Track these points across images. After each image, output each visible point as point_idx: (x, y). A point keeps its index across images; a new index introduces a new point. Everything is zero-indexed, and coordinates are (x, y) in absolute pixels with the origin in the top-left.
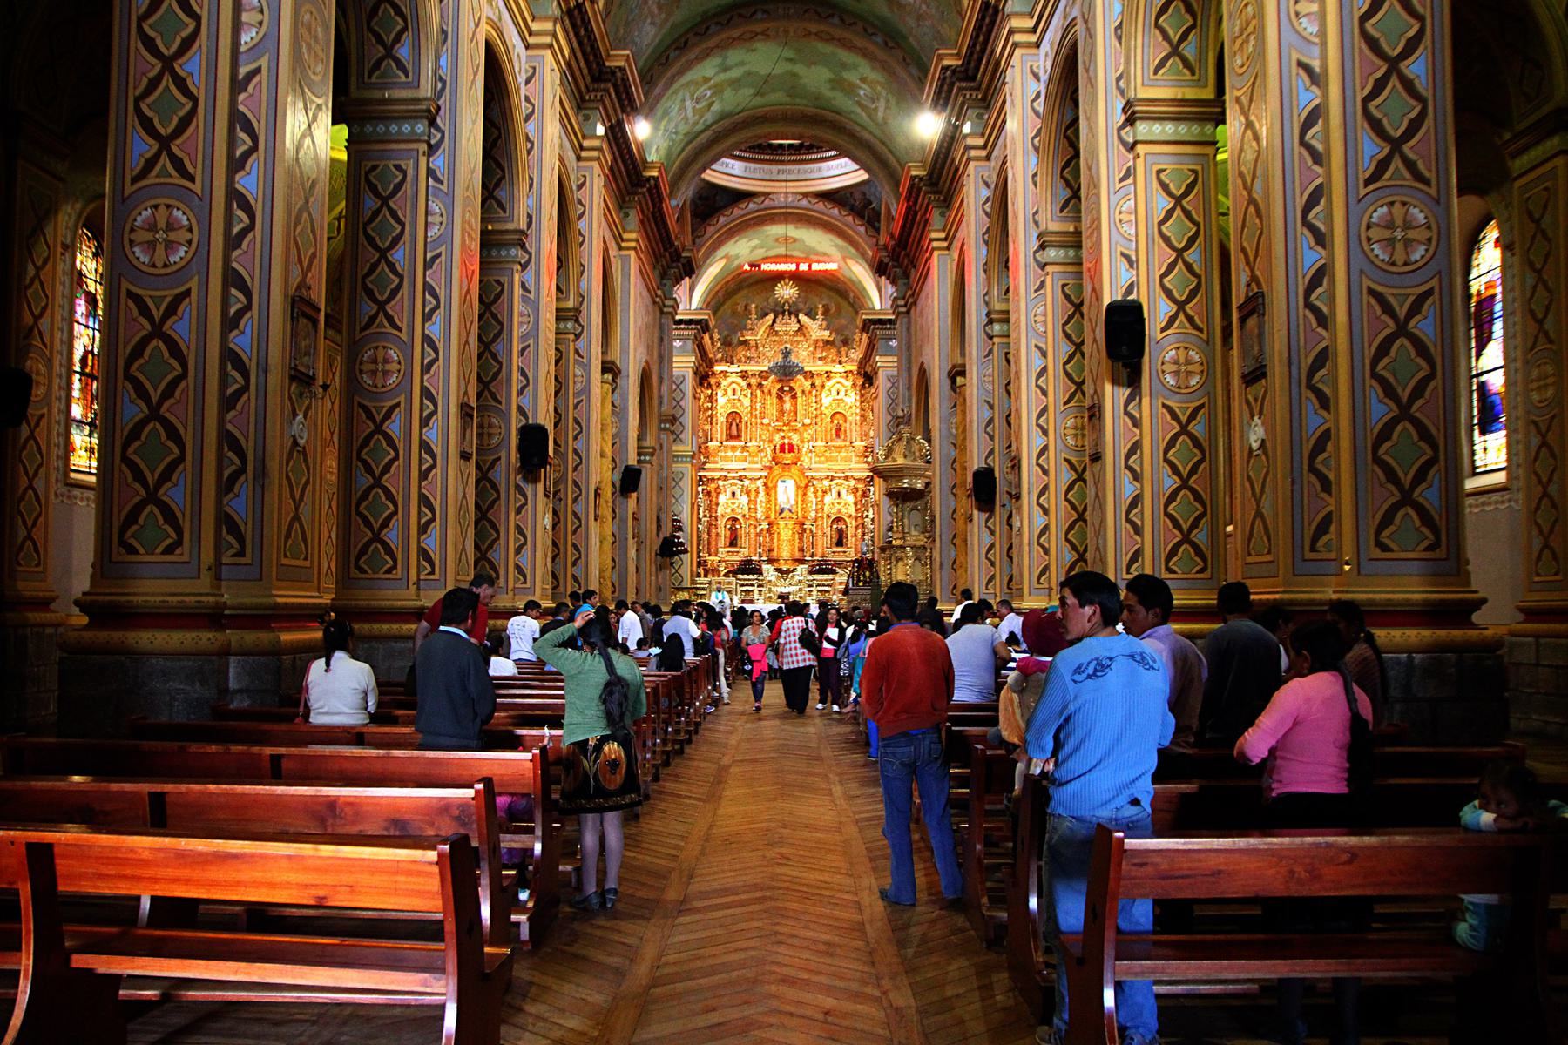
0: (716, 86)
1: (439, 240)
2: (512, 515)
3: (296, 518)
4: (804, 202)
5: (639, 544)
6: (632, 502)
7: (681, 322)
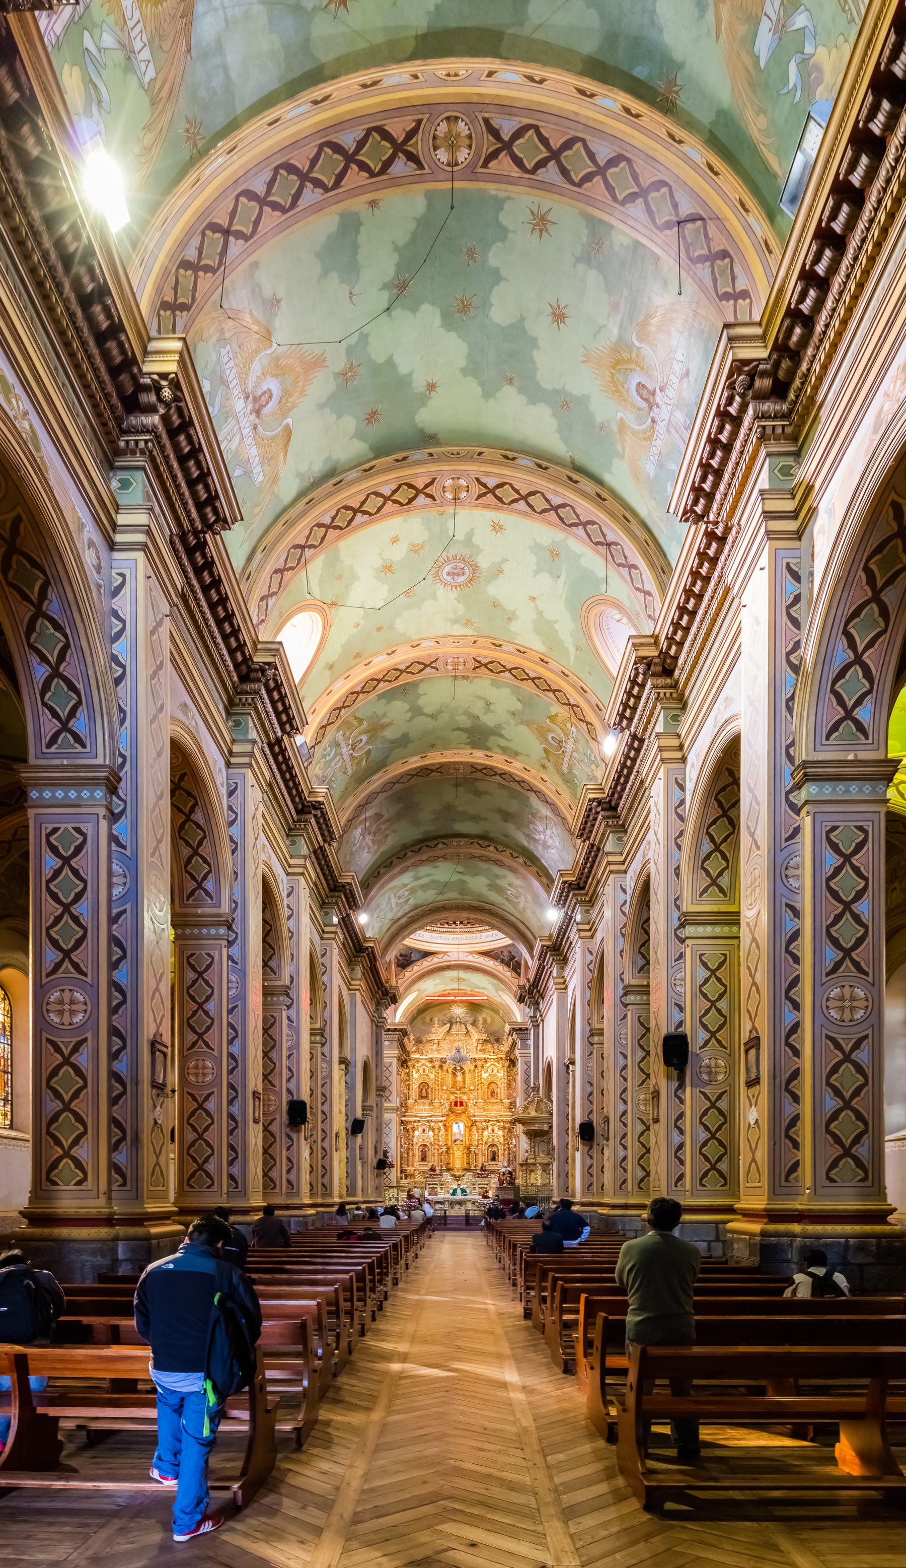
0: (411, 889)
1: (235, 998)
2: (284, 1151)
3: (157, 1164)
4: (470, 958)
5: (364, 1163)
6: (359, 1139)
7: (389, 1030)
